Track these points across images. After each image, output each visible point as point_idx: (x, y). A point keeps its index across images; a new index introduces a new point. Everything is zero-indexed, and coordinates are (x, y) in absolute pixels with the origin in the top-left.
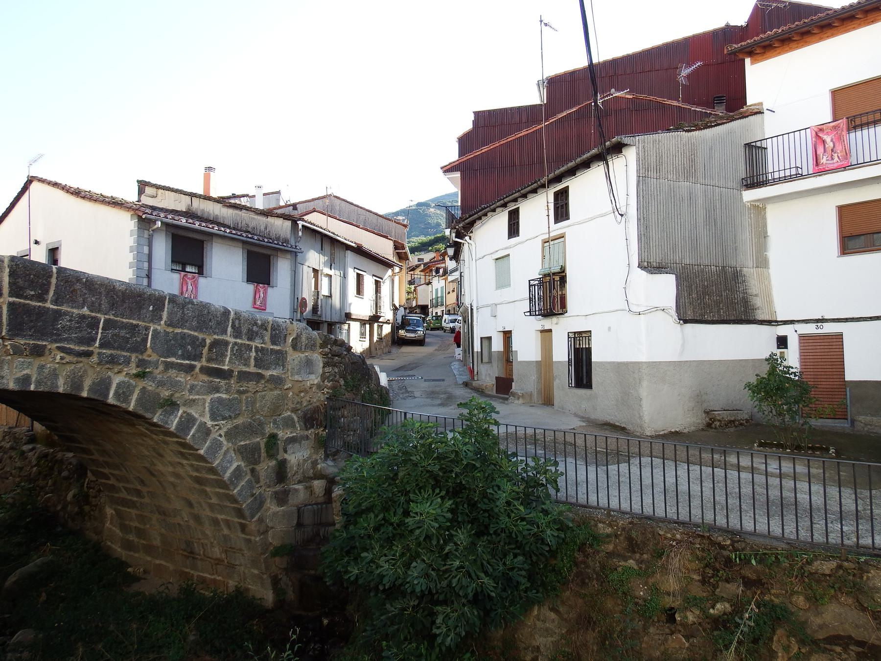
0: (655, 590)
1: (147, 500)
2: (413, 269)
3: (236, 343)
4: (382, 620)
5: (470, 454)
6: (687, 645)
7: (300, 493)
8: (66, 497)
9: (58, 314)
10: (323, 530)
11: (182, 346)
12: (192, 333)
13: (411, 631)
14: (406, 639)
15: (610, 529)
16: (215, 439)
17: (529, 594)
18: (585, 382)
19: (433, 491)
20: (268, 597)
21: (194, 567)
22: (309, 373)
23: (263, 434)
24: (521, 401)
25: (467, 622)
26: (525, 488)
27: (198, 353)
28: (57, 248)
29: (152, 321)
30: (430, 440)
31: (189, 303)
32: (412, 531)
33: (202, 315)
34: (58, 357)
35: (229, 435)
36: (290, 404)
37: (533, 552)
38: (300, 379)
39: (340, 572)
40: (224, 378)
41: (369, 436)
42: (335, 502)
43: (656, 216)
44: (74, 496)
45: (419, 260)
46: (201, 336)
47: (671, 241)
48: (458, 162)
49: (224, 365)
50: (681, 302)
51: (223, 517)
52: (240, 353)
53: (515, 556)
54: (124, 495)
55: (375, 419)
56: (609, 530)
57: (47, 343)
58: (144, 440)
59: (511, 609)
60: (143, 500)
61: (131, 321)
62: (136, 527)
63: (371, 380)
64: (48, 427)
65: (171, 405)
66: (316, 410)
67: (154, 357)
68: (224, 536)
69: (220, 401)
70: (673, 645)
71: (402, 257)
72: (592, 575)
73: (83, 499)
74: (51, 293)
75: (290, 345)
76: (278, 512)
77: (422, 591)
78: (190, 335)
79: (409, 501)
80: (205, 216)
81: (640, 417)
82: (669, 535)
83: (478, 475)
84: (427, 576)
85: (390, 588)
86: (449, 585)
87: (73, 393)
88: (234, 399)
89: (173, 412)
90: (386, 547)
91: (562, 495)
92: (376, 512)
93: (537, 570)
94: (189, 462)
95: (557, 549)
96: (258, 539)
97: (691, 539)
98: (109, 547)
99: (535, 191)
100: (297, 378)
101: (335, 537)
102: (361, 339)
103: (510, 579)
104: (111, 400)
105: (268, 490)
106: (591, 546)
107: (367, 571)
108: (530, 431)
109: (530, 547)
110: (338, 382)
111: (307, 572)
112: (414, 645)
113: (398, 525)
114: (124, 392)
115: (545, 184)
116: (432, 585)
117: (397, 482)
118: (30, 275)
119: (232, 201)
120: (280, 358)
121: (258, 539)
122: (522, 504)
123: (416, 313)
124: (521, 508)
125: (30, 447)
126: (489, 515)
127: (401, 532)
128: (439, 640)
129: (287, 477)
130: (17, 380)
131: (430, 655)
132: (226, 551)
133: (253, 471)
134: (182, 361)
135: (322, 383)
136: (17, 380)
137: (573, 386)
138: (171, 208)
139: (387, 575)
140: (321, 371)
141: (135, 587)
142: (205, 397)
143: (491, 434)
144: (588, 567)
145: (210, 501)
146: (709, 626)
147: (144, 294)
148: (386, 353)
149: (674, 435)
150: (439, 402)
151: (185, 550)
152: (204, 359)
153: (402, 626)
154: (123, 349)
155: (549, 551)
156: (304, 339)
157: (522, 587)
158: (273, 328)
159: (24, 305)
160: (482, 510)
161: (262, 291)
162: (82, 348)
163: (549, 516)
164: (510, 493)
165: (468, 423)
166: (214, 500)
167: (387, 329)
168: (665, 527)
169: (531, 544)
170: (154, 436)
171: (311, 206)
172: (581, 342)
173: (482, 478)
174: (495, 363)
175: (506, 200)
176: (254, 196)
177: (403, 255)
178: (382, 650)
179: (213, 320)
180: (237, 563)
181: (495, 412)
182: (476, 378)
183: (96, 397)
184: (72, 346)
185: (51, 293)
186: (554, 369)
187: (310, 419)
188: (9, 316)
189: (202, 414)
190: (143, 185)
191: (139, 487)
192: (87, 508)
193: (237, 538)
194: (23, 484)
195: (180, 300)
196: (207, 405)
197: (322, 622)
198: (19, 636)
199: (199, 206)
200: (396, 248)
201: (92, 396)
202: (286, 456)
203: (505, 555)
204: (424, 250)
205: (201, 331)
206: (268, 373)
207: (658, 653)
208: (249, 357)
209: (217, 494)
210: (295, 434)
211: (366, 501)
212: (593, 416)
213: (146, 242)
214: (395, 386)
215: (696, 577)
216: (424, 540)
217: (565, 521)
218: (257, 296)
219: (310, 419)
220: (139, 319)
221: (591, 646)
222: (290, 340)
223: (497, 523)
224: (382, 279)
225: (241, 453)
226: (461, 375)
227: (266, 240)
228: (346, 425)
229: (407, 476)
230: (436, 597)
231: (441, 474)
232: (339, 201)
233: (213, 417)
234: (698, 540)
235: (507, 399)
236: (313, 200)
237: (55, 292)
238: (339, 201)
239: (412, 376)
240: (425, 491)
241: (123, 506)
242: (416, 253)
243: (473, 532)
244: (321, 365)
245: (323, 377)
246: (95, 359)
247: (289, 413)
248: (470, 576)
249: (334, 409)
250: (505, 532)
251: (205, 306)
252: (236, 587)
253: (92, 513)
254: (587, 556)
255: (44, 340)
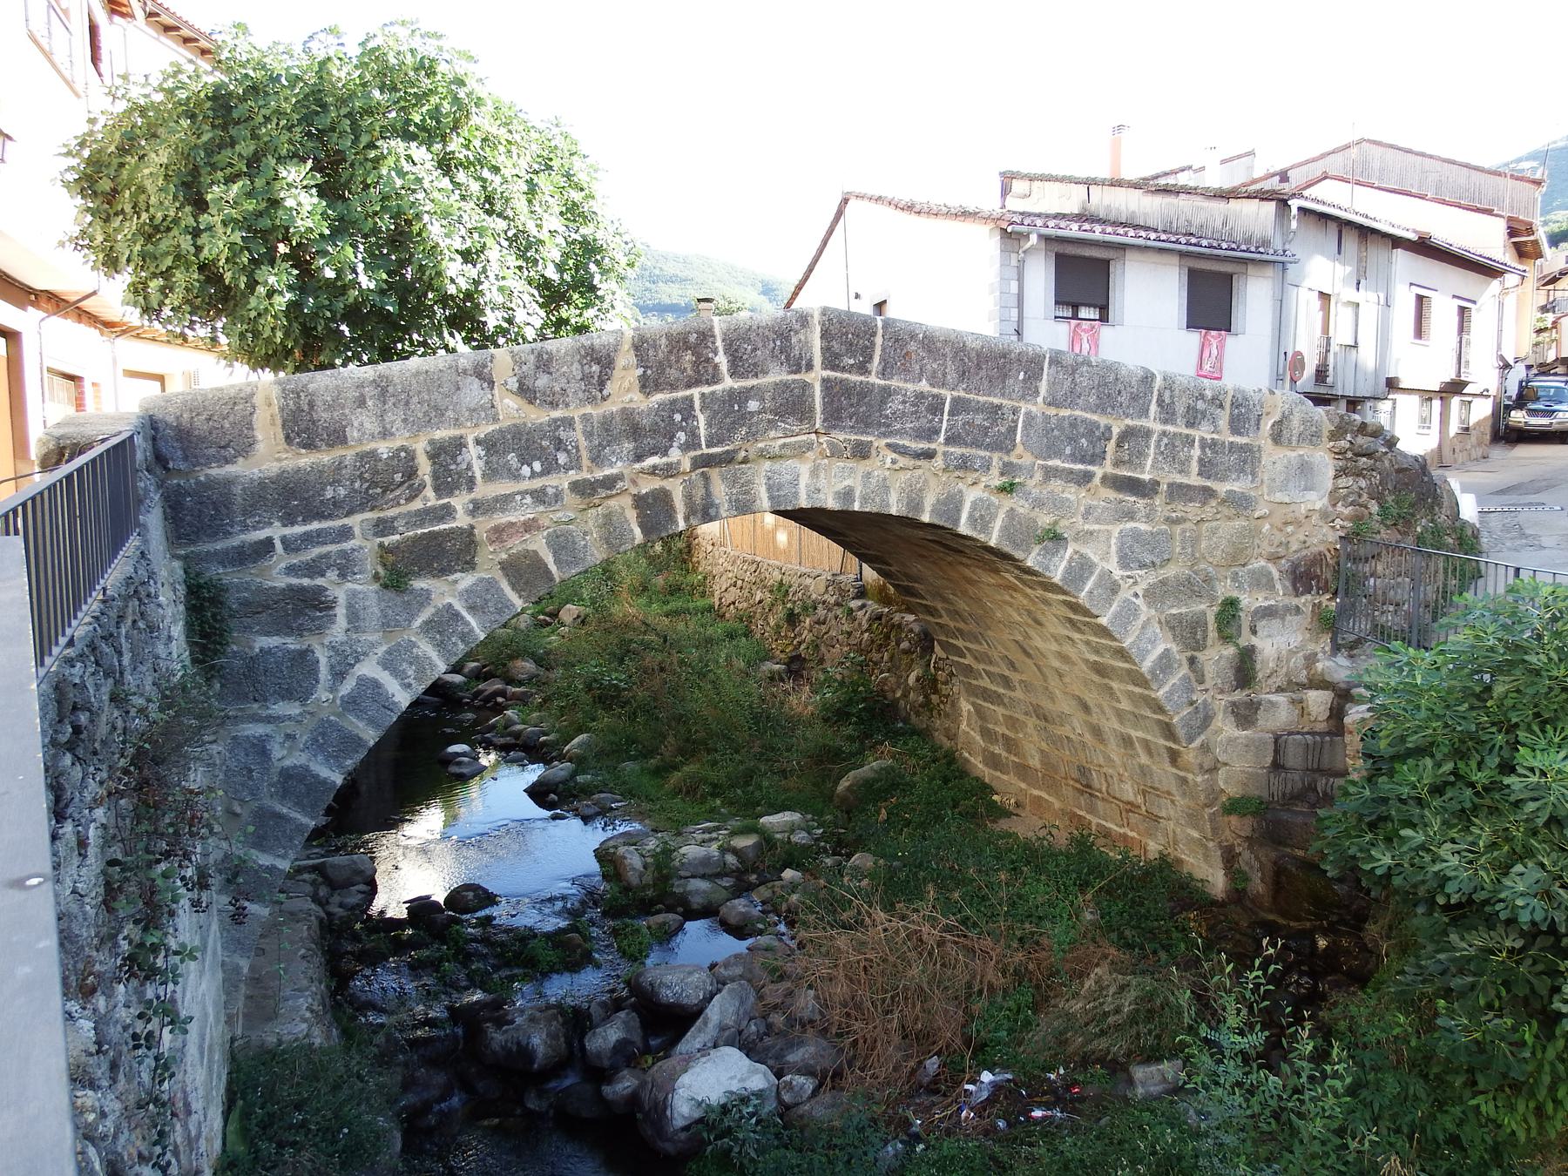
1: (1018, 694)
3: (1164, 433)
4: (1439, 961)
7: (1279, 713)
8: (906, 680)
9: (887, 393)
10: (1324, 781)
11: (1071, 439)
12: (1088, 416)
14: (1490, 1007)
16: (1126, 600)
20: (1216, 881)
22: (1306, 489)
23: (1213, 599)
27: (1098, 451)
28: (885, 301)
29: (1023, 397)
31: (1083, 363)
32: (1517, 804)
33: (1105, 384)
34: (889, 460)
35: (1151, 595)
36: (1265, 545)
38: (1287, 500)
39: (1354, 857)
40: (1144, 496)
41: (1428, 617)
42: (1351, 733)
44: (918, 680)
46: (1103, 421)
51: (1140, 734)
52: (1172, 450)
54: (985, 682)
55: (1445, 585)
58: (1012, 597)
60: (1012, 694)
61: (991, 399)
64: (879, 572)
65: (1054, 538)
66: (1318, 559)
67: (1027, 460)
68: (1141, 767)
69: (1136, 536)
71: (1525, 251)
73: (930, 684)
75: (1267, 435)
76: (1237, 738)
77: (1534, 923)
78: (1084, 421)
80: (1112, 217)
85: (1459, 905)
88: (1160, 533)
90: (1455, 826)
92: (1439, 756)
94: (1083, 637)
98: (967, 760)
101: (1346, 794)
102: (1421, 431)
104: (964, 528)
105: (1220, 697)
107: (1412, 866)
110: (1366, 508)
111: (1289, 850)
112: (1509, 1022)
113: (1485, 789)
114: (982, 519)
117: (1488, 704)
119: (1162, 181)
120: (1247, 459)
123: (1556, 374)
125: (859, 603)
127: (1492, 803)
129: (1255, 678)
131: (1544, 1049)
132: (1144, 793)
133: (1192, 661)
134: (1072, 466)
135: (1330, 509)
138: (1053, 211)
139: (1456, 877)
140: (1329, 485)
141: (1004, 825)
142: (1109, 527)
147: (1011, 352)
148: (1477, 459)
151: (1076, 781)
152: (1108, 462)
153: (1482, 980)
154: (979, 446)
156: (1295, 422)
158: (1235, 404)
161: (1214, 343)
162: (921, 446)
166: (1125, 705)
167: (1482, 410)
170: (1029, 591)
171: (1316, 170)
176: (1203, 168)
177: (1529, 248)
178: (1436, 1015)
179: (1123, 393)
180: (1163, 814)
184: (907, 443)
185: (876, 359)
187: (1304, 577)
189: (1105, 557)
190: (1008, 179)
191: (1007, 673)
193: (1164, 772)
196: (1113, 541)
197: (1314, 943)
199: (1104, 200)
200: (1512, 232)
201: (937, 521)
202: (1255, 641)
205: (1104, 412)
206: (1222, 488)
208: (1189, 458)
209: (1130, 695)
210: (1272, 602)
211: (1416, 733)
214: (1495, 522)
216: (1547, 824)
219: (1304, 577)
222: (1267, 425)
224: (1474, 302)
225: (1172, 628)
227: (1224, 245)
228: (1380, 592)
229: (1514, 695)
233: (1124, 562)
236: (1323, 156)
237: (882, 359)
238: (1380, 149)
239: (1538, 504)
240: (1555, 730)
241: (985, 700)
244: (1331, 473)
245: (1335, 497)
246: (939, 462)
247: (1263, 563)
249: (1356, 560)
251: (1111, 368)
253: (942, 706)
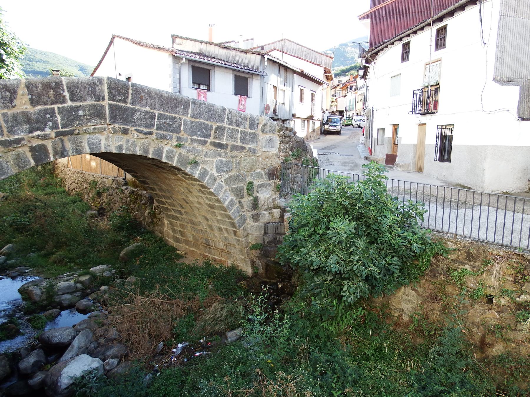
0: (482, 284)
1: (184, 216)
2: (335, 87)
3: (229, 128)
4: (312, 286)
5: (368, 196)
6: (498, 317)
7: (266, 217)
9: (134, 111)
13: (328, 292)
14: (325, 297)
15: (455, 246)
17: (400, 279)
18: (446, 158)
19: (344, 217)
20: (249, 270)
21: (210, 253)
23: (245, 182)
24: (401, 169)
25: (361, 291)
26: (402, 218)
29: (183, 114)
30: (344, 186)
31: (203, 104)
32: (330, 238)
33: (211, 111)
34: (136, 135)
35: (227, 181)
36: (260, 165)
37: (404, 256)
38: (266, 150)
40: (224, 149)
42: (286, 221)
43: (510, 44)
44: (148, 214)
45: (339, 81)
47: (520, 63)
48: (369, 12)
49: (223, 141)
50: (522, 105)
51: (224, 227)
52: (232, 134)
53: (393, 257)
54: (173, 213)
56: (455, 247)
57: (129, 127)
59: (388, 286)
60: (182, 216)
61: (172, 115)
62: (180, 231)
63: (308, 152)
65: (195, 163)
66: (275, 169)
67: (185, 136)
68: (225, 237)
69: (221, 162)
70: (489, 316)
71: (328, 78)
72: (441, 272)
73: (153, 215)
74: (130, 98)
78: (204, 123)
79: (329, 222)
81: (482, 182)
82: (495, 253)
83: (373, 208)
84: (339, 263)
85: (317, 269)
86: (352, 269)
87: (144, 155)
88: (229, 161)
89: (196, 168)
90: (315, 246)
91: (425, 224)
92: (310, 226)
93: (406, 266)
94: (205, 196)
95: (420, 255)
96: (243, 239)
97: (510, 256)
98: (167, 240)
99: (422, 29)
100: (264, 150)
101: (286, 240)
103: (388, 270)
104: (164, 160)
106: (442, 255)
108: (408, 186)
109: (402, 253)
111: (269, 259)
112: (330, 300)
115: (430, 23)
116: (341, 269)
118: (118, 88)
119: (226, 45)
120: (254, 137)
121: (243, 239)
122: (399, 227)
123: (336, 115)
124: (399, 229)
125: (125, 187)
126: (378, 232)
127: (324, 238)
128: (344, 299)
130: (117, 148)
132: (226, 245)
133: (240, 202)
134: (200, 139)
136: (117, 148)
137: (438, 160)
138: (190, 51)
139: (316, 261)
141: (181, 261)
142: (213, 159)
143: (382, 184)
144: (439, 267)
145: (217, 218)
146: (514, 308)
147: (178, 98)
149: (506, 195)
150: (349, 168)
151: (205, 244)
152: (212, 137)
154: (168, 131)
155: (415, 256)
156: (268, 126)
157: (396, 275)
159: (116, 105)
160: (374, 229)
161: (243, 100)
162: (148, 130)
163: (416, 235)
164: (392, 220)
165: (368, 177)
166: (219, 218)
167: (318, 125)
168: (493, 247)
169: (403, 251)
170: (187, 181)
172: (446, 132)
173: (375, 210)
174: (386, 146)
175: (401, 36)
176: (238, 42)
177: (329, 77)
178: (311, 301)
179: (216, 114)
180: (232, 252)
181: (386, 171)
182: (373, 154)
183: (156, 158)
184: (142, 129)
185: (130, 98)
186: (426, 149)
187: (271, 175)
188: (110, 113)
190: (174, 38)
191: (180, 209)
192: (155, 220)
193: (232, 238)
194: (123, 206)
195: (198, 102)
196: (214, 164)
197: (278, 286)
198: (129, 279)
200: (325, 72)
201: (154, 157)
202: (258, 195)
203: (386, 256)
204: (343, 75)
205: (210, 121)
206: (247, 146)
207: (478, 320)
208: (237, 137)
209: (221, 214)
210: (263, 183)
212: (449, 180)
213: (177, 71)
214: (322, 157)
215: (510, 279)
216: (338, 243)
217: (426, 239)
218: (240, 104)
219: (271, 175)
220: (176, 113)
221: (436, 312)
222: (260, 127)
223: (383, 237)
225: (233, 192)
226: (363, 152)
230: (343, 275)
231: (350, 207)
232: (290, 42)
233: (218, 171)
234: (515, 257)
235: (392, 168)
236: (274, 43)
237: (132, 98)
241: (173, 219)
242: (337, 77)
243: (367, 241)
244: (279, 142)
246: (154, 136)
247: (260, 170)
248: (364, 266)
250: (387, 243)
251: (212, 106)
252: (232, 264)
253: (158, 222)
254: (438, 261)
255: (127, 125)
